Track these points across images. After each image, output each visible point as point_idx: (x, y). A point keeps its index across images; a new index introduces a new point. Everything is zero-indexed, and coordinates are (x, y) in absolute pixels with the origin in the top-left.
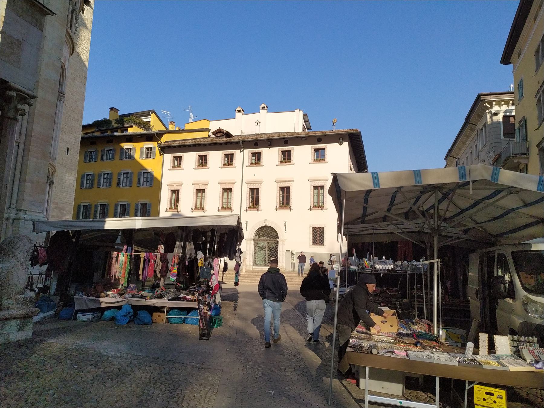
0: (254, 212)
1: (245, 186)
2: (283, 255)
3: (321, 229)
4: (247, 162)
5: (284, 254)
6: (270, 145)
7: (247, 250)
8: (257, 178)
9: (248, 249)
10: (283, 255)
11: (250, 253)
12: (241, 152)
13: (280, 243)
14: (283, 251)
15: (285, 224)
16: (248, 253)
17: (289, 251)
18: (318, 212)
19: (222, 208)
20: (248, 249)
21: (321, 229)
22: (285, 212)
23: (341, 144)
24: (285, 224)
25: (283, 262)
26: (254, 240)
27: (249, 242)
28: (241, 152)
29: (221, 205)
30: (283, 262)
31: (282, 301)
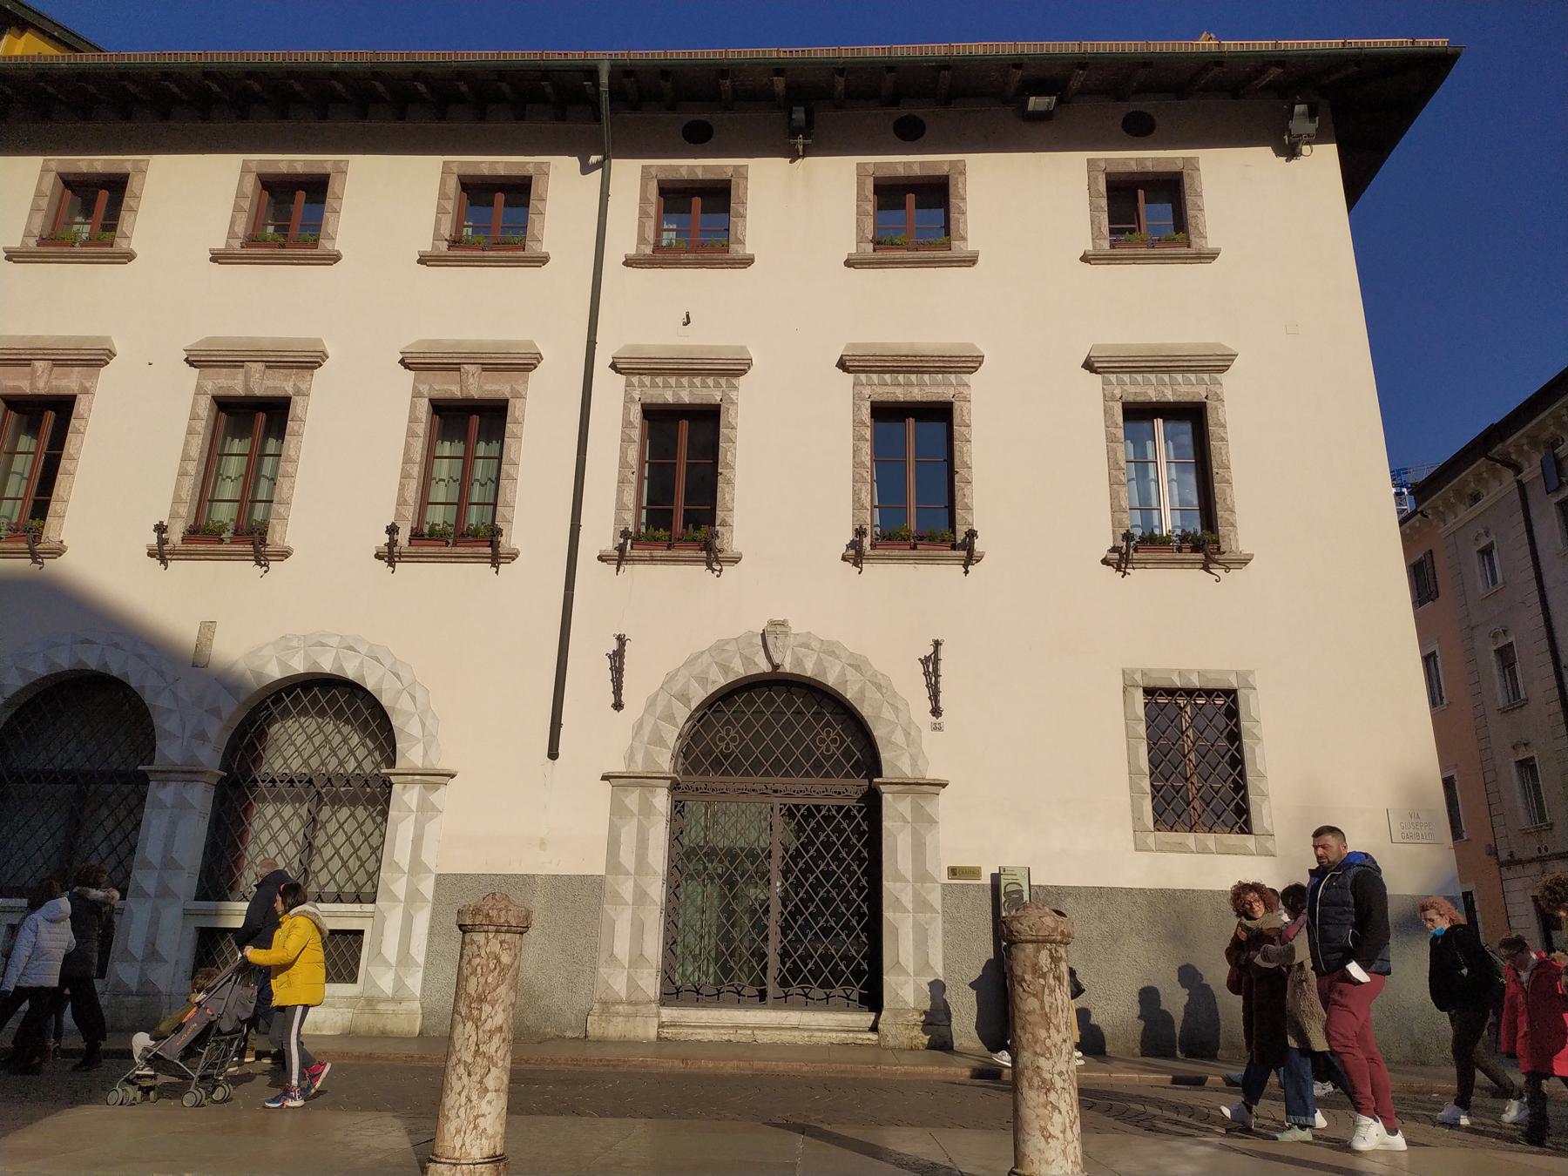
0: (669, 582)
1: (603, 374)
2: (922, 904)
3: (1224, 706)
4: (625, 235)
5: (935, 898)
6: (807, 129)
7: (613, 864)
8: (709, 337)
9: (627, 858)
10: (922, 904)
11: (641, 896)
12: (586, 169)
13: (896, 811)
14: (922, 876)
15: (931, 664)
16: (627, 889)
17: (974, 872)
18: (1172, 586)
19: (416, 535)
20: (627, 858)
21: (1224, 706)
22: (915, 587)
23: (1290, 151)
24: (931, 664)
25: (405, 958)
26: (675, 787)
27: (632, 799)
28: (586, 169)
29: (410, 512)
30: (405, 958)
31: (923, 128)
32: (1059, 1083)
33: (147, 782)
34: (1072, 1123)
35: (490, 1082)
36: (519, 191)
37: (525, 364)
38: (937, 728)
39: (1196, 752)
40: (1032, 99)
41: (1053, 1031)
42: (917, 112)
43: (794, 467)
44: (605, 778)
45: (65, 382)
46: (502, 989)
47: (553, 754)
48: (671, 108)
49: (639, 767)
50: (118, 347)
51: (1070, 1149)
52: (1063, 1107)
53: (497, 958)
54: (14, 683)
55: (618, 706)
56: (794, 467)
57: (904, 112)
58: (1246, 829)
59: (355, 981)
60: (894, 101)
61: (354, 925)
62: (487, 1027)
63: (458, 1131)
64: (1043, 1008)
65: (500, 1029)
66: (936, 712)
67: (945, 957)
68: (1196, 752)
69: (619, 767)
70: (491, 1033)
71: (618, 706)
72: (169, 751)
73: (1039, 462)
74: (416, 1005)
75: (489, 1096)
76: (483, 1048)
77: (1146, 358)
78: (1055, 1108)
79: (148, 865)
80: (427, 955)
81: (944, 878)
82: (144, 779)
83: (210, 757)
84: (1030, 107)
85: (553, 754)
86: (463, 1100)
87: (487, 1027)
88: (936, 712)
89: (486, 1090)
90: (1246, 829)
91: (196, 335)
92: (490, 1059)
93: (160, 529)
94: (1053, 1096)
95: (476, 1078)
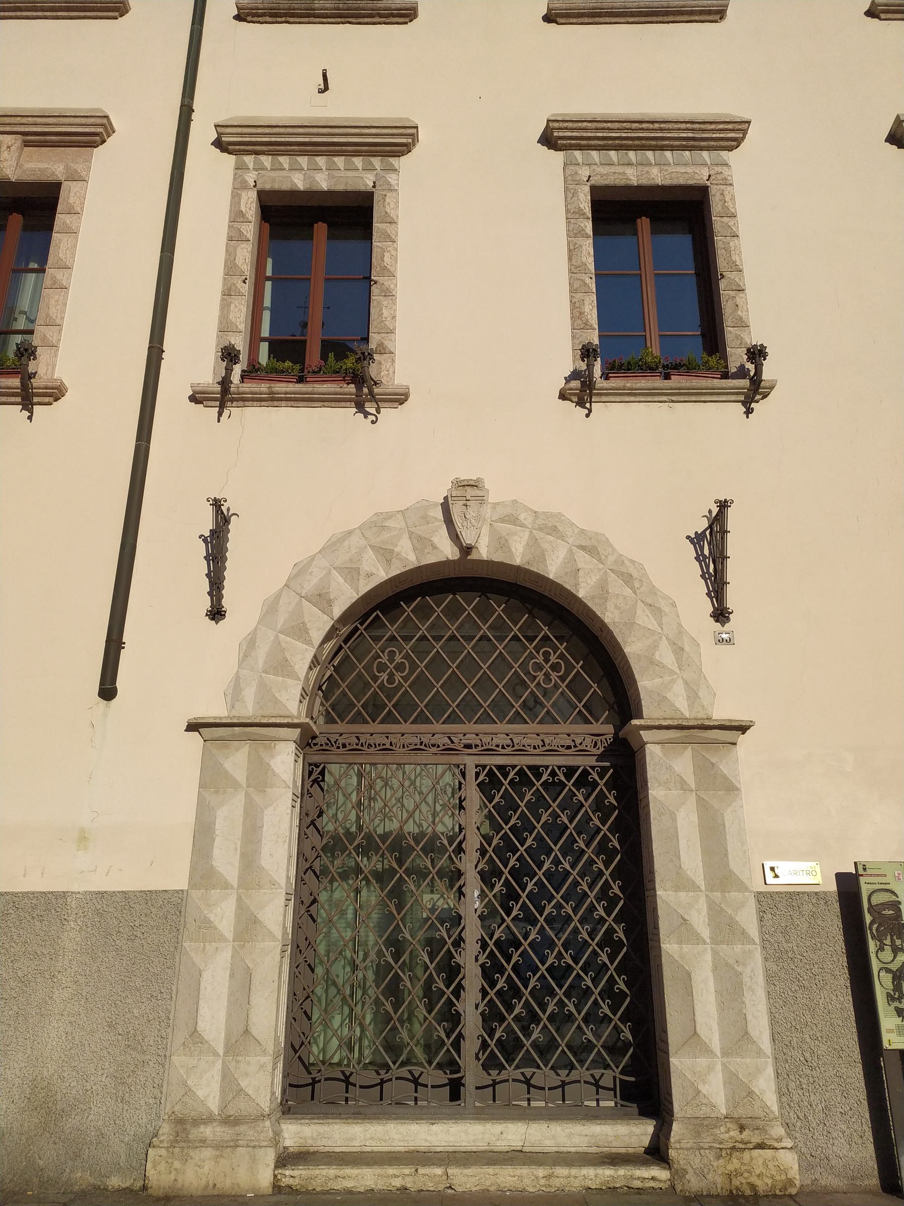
49: (248, 710)
55: (216, 613)
67: (773, 1022)
69: (217, 710)
71: (216, 613)
85: (108, 691)
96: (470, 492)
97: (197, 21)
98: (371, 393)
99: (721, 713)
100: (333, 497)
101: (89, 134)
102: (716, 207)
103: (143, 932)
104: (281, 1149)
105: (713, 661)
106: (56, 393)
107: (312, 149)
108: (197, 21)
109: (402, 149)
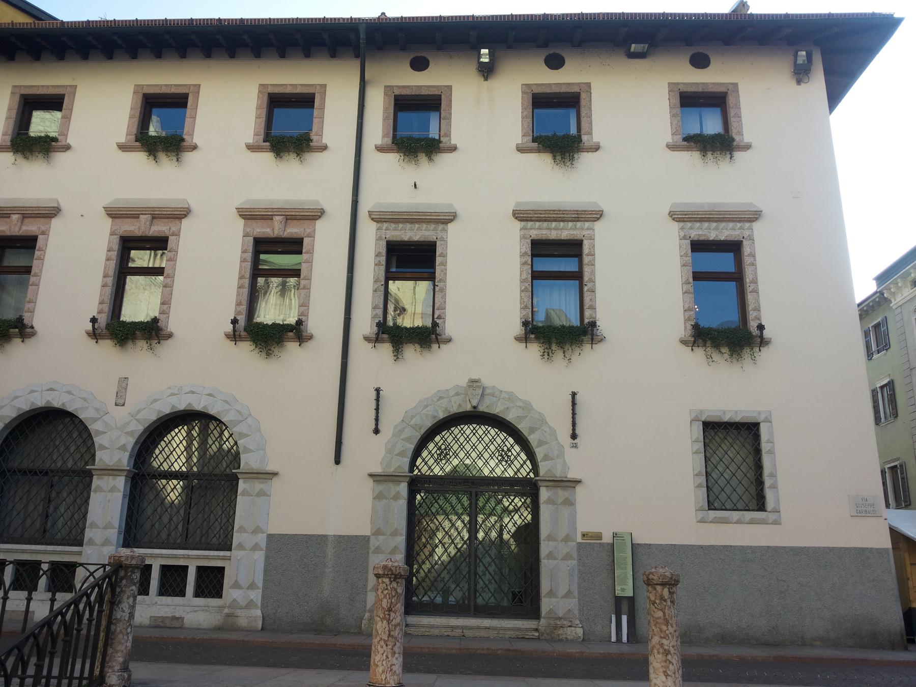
17: (598, 536)
32: (672, 651)
33: (91, 476)
34: (678, 670)
35: (396, 649)
36: (305, 101)
37: (316, 215)
38: (575, 446)
39: (734, 455)
40: (633, 46)
41: (670, 627)
42: (558, 51)
43: (484, 282)
44: (371, 475)
45: (30, 228)
46: (399, 605)
47: (337, 461)
48: (403, 49)
49: (391, 470)
50: (63, 206)
51: (677, 681)
52: (674, 661)
53: (396, 590)
54: (10, 413)
55: (376, 431)
56: (484, 282)
57: (551, 52)
58: (761, 507)
59: (184, 596)
60: (545, 45)
61: (219, 564)
62: (393, 623)
63: (383, 672)
64: (664, 615)
65: (399, 624)
66: (574, 436)
67: (579, 587)
68: (734, 455)
69: (378, 470)
70: (396, 626)
71: (376, 431)
72: (103, 457)
73: (639, 284)
74: (259, 613)
75: (397, 655)
76: (392, 633)
77: (705, 213)
78: (670, 662)
79: (94, 525)
80: (264, 583)
81: (579, 539)
82: (89, 475)
83: (124, 459)
84: (632, 50)
85: (337, 461)
86: (385, 657)
87: (393, 623)
88: (574, 436)
89: (395, 653)
90: (761, 507)
91: (108, 200)
92: (396, 638)
93: (94, 320)
94: (669, 657)
95: (389, 647)
96: (475, 384)
97: (117, 310)
98: (437, 339)
99: (571, 475)
100: (418, 384)
101: (316, 215)
102: (439, 251)
103: (353, 547)
104: (138, 144)
105: (570, 455)
106: (311, 337)
107: (412, 221)
108: (117, 310)
109: (446, 222)
